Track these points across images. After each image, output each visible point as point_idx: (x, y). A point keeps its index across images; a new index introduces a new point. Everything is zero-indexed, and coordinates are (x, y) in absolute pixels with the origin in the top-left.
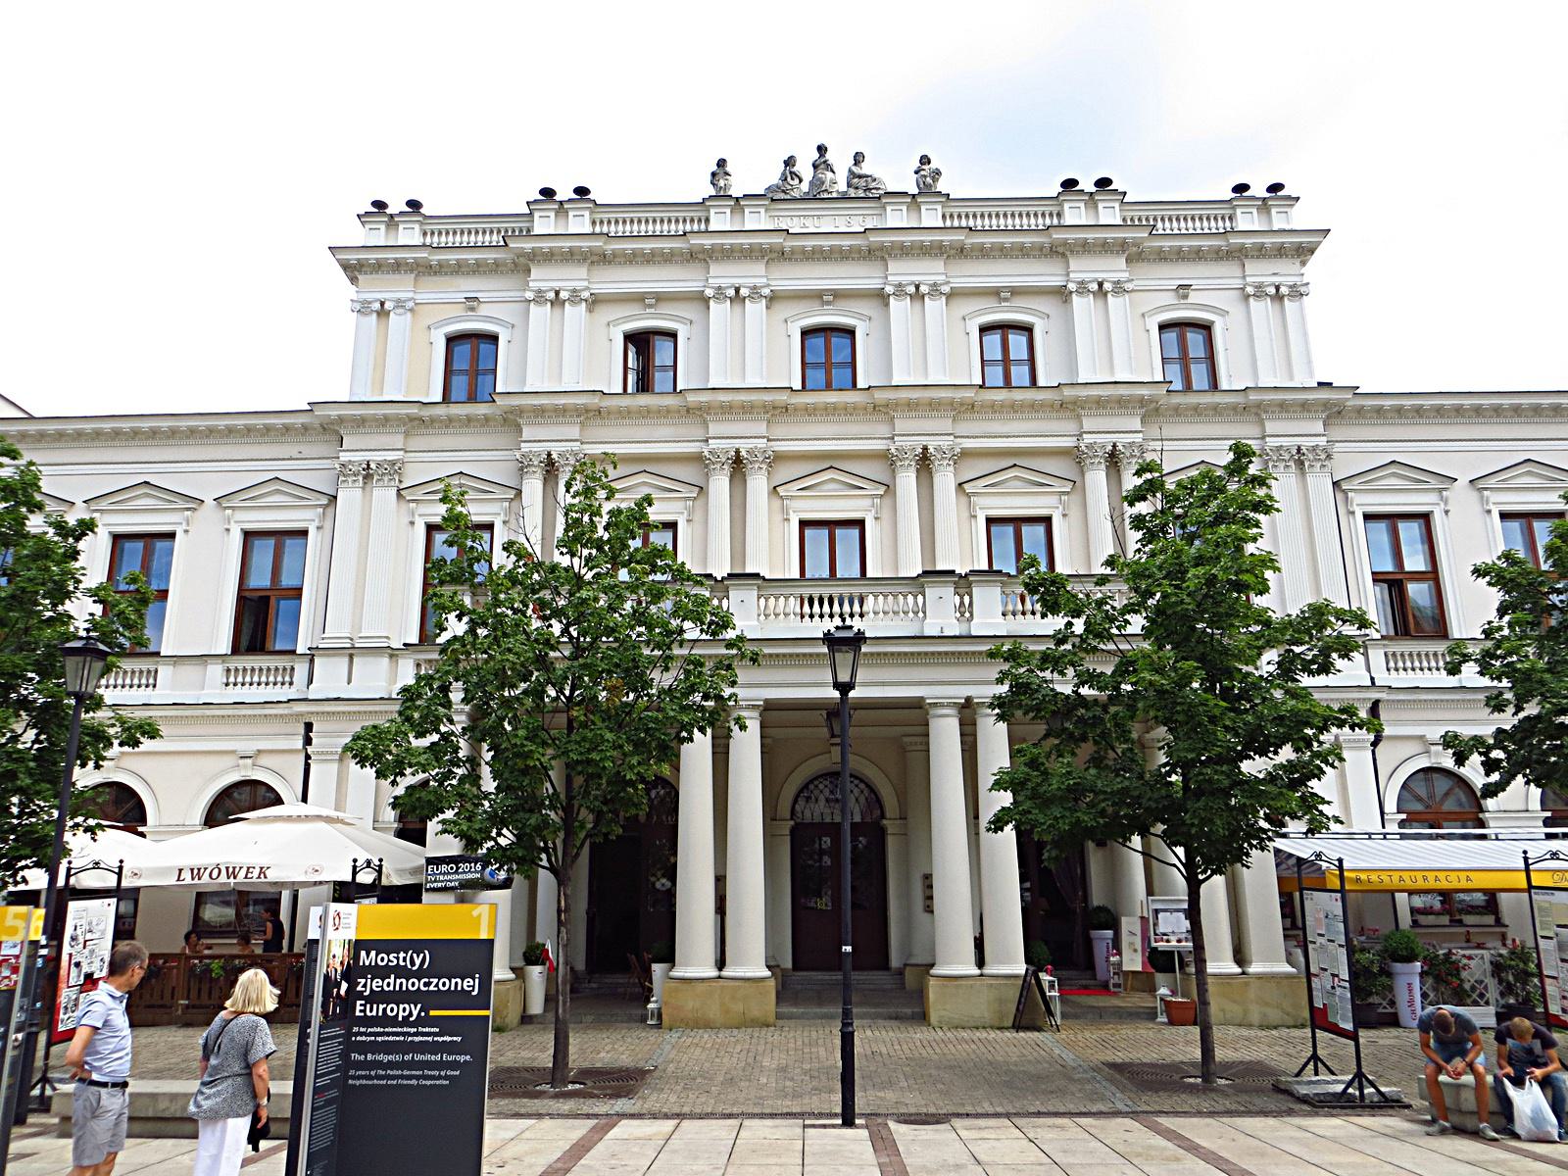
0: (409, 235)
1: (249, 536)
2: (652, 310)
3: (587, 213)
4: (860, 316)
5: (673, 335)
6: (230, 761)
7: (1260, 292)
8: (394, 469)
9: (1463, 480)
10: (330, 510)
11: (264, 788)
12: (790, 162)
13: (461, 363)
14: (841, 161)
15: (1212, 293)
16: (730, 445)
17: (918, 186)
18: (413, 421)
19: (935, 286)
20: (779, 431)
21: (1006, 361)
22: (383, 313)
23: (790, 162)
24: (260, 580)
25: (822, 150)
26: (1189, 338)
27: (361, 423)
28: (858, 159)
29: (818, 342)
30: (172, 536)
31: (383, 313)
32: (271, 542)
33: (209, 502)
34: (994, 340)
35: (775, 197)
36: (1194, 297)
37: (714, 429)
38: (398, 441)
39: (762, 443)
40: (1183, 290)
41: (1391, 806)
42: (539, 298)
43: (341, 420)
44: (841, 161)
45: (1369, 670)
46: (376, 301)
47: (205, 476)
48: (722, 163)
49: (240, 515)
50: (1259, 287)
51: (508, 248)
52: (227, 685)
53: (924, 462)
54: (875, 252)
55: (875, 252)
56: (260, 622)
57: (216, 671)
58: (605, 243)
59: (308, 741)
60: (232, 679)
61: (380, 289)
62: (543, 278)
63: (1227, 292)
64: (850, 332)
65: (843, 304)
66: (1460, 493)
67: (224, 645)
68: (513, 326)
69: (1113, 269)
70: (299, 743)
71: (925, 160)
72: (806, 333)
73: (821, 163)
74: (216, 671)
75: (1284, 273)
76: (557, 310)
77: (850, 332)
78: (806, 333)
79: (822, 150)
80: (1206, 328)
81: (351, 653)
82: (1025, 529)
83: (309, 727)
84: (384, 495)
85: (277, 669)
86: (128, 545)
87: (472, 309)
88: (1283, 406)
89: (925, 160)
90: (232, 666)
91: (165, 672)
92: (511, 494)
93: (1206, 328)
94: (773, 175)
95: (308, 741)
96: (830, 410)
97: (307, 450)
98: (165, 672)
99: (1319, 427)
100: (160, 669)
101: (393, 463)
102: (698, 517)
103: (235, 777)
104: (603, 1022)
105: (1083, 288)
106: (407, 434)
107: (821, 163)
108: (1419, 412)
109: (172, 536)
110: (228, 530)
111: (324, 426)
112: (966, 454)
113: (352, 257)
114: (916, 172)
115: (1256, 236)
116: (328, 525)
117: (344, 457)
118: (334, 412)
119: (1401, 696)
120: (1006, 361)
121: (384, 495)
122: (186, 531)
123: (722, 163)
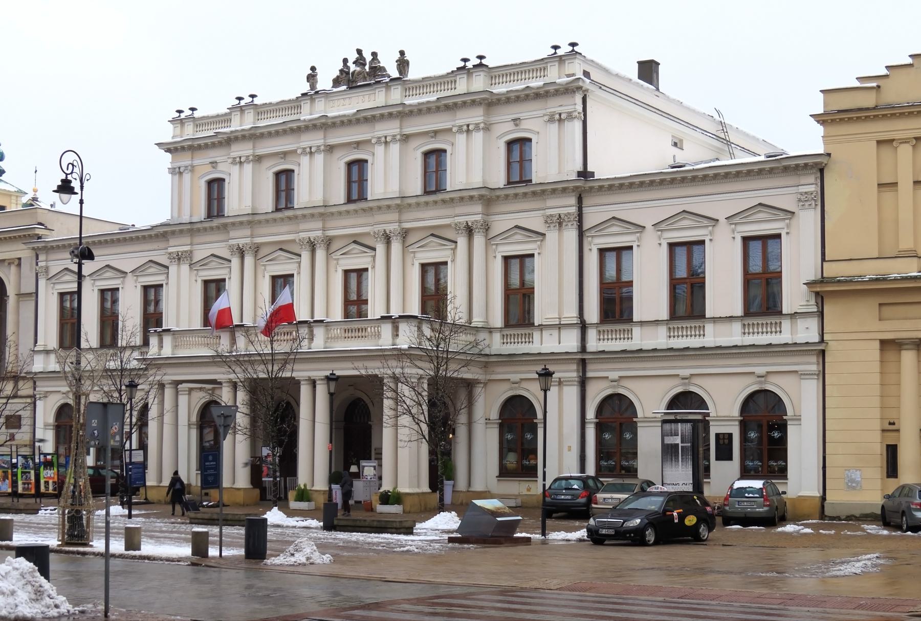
4: (445, 142)
6: (677, 381)
11: (762, 395)
12: (345, 61)
13: (516, 156)
18: (191, 230)
19: (477, 125)
22: (180, 173)
23: (345, 61)
24: (756, 266)
26: (518, 148)
28: (374, 55)
30: (631, 248)
33: (722, 220)
36: (525, 125)
38: (187, 240)
39: (248, 240)
40: (516, 121)
41: (591, 414)
44: (369, 58)
47: (720, 203)
52: (744, 333)
60: (747, 330)
61: (185, 160)
65: (440, 137)
69: (475, 116)
73: (360, 61)
79: (359, 52)
83: (35, 383)
85: (776, 323)
86: (608, 254)
90: (746, 323)
91: (636, 331)
98: (636, 331)
100: (634, 329)
103: (755, 388)
105: (379, 141)
107: (360, 61)
108: (631, 185)
109: (532, 255)
110: (660, 244)
111: (159, 234)
115: (561, 86)
119: (677, 353)
121: (185, 268)
122: (711, 240)
123: (313, 69)
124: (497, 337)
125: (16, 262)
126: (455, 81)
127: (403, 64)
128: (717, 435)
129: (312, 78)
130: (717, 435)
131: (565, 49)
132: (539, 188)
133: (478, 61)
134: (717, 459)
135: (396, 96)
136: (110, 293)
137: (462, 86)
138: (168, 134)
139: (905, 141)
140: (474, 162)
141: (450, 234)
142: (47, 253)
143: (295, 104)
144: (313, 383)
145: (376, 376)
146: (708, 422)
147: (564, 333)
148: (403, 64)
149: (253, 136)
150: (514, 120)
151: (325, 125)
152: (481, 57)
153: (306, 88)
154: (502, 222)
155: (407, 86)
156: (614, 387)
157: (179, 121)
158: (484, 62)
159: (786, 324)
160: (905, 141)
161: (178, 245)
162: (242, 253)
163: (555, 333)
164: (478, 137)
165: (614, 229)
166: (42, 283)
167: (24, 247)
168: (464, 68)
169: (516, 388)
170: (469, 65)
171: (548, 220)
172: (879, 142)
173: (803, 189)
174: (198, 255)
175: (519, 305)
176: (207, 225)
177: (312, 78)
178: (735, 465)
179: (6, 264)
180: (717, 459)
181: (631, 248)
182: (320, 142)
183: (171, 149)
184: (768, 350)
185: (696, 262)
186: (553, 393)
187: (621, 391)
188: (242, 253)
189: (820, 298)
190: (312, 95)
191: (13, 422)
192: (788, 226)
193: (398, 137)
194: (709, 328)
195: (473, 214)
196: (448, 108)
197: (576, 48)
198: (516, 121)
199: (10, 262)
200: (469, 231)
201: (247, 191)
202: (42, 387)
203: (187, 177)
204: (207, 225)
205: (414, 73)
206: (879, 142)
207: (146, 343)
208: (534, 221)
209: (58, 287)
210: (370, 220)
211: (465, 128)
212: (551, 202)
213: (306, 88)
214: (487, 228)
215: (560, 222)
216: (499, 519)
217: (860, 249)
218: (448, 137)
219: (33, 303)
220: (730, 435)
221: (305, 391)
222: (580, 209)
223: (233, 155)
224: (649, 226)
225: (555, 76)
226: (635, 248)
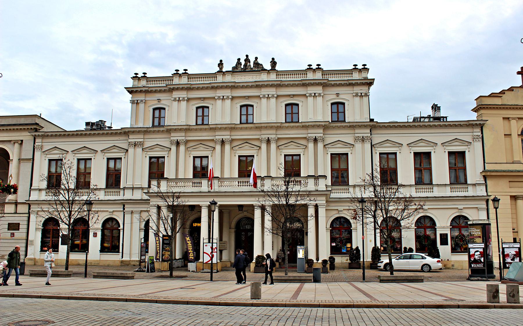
0: (143, 83)
1: (50, 161)
4: (255, 102)
5: (208, 107)
7: (357, 95)
8: (141, 144)
9: (405, 144)
10: (127, 153)
12: (239, 59)
13: (335, 110)
14: (252, 60)
15: (345, 95)
16: (267, 136)
20: (233, 133)
21: (247, 115)
22: (137, 103)
23: (239, 59)
25: (247, 56)
26: (338, 107)
27: (133, 132)
28: (256, 58)
29: (335, 106)
30: (91, 159)
31: (137, 103)
32: (84, 161)
34: (335, 106)
35: (235, 70)
36: (162, 102)
37: (172, 135)
38: (142, 136)
40: (338, 94)
42: (175, 100)
43: (129, 131)
44: (252, 60)
45: (487, 191)
48: (221, 61)
49: (149, 153)
51: (168, 86)
53: (268, 141)
54: (258, 86)
55: (258, 86)
56: (113, 179)
57: (44, 193)
59: (124, 209)
61: (140, 97)
62: (176, 94)
64: (298, 105)
65: (295, 98)
66: (405, 148)
67: (104, 187)
69: (318, 90)
70: (122, 210)
71: (273, 59)
72: (286, 105)
73: (247, 60)
74: (102, 192)
75: (362, 90)
76: (361, 98)
77: (298, 105)
78: (286, 105)
79: (247, 56)
80: (343, 104)
81: (133, 189)
82: (203, 159)
83: (124, 206)
84: (139, 150)
86: (81, 161)
87: (338, 96)
88: (175, 130)
92: (169, 150)
93: (343, 104)
95: (124, 209)
96: (293, 127)
97: (121, 138)
99: (321, 131)
101: (141, 142)
102: (306, 153)
104: (293, 271)
106: (144, 134)
107: (247, 60)
111: (125, 133)
112: (279, 139)
113: (130, 90)
115: (359, 80)
116: (126, 157)
117: (130, 140)
118: (127, 130)
120: (247, 115)
121: (139, 150)
123: (221, 61)
124: (102, 192)
125: (20, 142)
127: (274, 63)
128: (441, 234)
129: (221, 64)
130: (441, 234)
131: (314, 67)
132: (114, 132)
134: (61, 244)
135: (273, 77)
136: (55, 162)
137: (310, 76)
138: (130, 83)
139: (514, 119)
140: (315, 109)
141: (257, 143)
142: (42, 138)
144: (263, 208)
145: (253, 205)
146: (436, 229)
147: (478, 187)
148: (274, 63)
150: (337, 94)
151: (234, 87)
153: (218, 69)
154: (330, 139)
156: (110, 214)
157: (135, 77)
159: (470, 188)
160: (514, 119)
161: (133, 139)
162: (178, 144)
163: (37, 192)
164: (319, 99)
165: (157, 149)
166: (38, 154)
167: (29, 134)
169: (461, 212)
171: (356, 139)
172: (503, 118)
173: (475, 134)
174: (147, 144)
175: (340, 177)
176: (152, 129)
177: (221, 64)
178: (448, 247)
179: (12, 142)
180: (61, 244)
181: (91, 159)
183: (131, 91)
184: (466, 198)
185: (88, 166)
186: (128, 217)
187: (114, 217)
188: (178, 144)
189: (485, 177)
191: (13, 227)
192: (304, 152)
193: (186, 99)
194: (435, 189)
195: (318, 133)
196: (213, 88)
198: (338, 94)
199: (15, 142)
200: (315, 140)
201: (179, 114)
202: (94, 208)
203: (142, 106)
204: (152, 129)
205: (278, 68)
206: (503, 118)
207: (149, 187)
208: (349, 139)
209: (48, 156)
210: (213, 134)
212: (357, 131)
214: (323, 140)
215: (363, 140)
216: (242, 273)
217: (498, 159)
219: (31, 164)
220: (447, 234)
221: (258, 213)
222: (482, 133)
223: (174, 96)
224: (99, 151)
225: (356, 76)
226: (93, 159)
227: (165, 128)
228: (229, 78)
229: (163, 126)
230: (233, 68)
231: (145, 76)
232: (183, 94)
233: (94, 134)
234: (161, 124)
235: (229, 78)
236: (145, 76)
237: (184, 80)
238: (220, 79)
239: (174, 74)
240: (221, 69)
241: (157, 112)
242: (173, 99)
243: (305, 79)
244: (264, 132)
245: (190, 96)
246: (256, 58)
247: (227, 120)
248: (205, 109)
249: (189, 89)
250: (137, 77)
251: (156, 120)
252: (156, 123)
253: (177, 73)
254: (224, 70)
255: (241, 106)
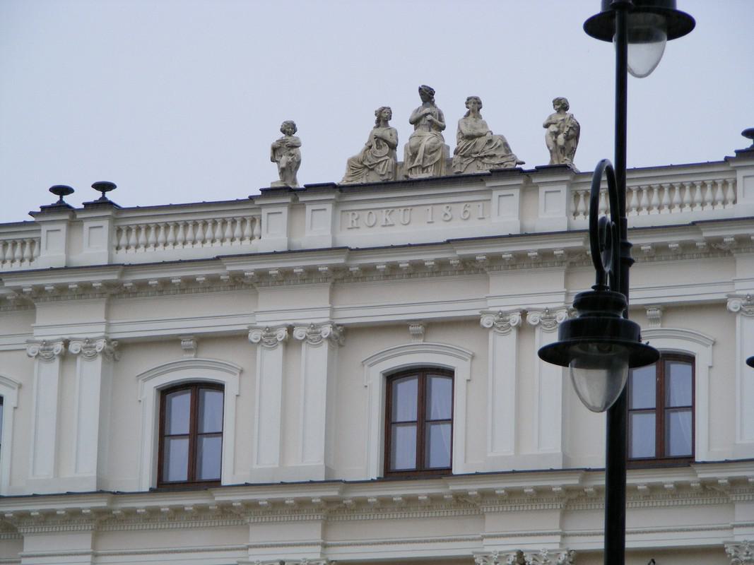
2: (420, 341)
3: (105, 223)
12: (383, 117)
17: (442, 136)
23: (383, 117)
25: (427, 95)
28: (474, 105)
42: (45, 352)
44: (452, 111)
46: (516, 311)
48: (289, 129)
50: (503, 316)
58: (348, 259)
62: (53, 324)
63: (12, 354)
65: (438, 338)
68: (20, 386)
73: (428, 119)
79: (427, 95)
89: (562, 106)
94: (356, 140)
107: (428, 119)
114: (547, 126)
123: (289, 129)
126: (735, 184)
129: (286, 149)
131: (82, 195)
133: (96, 195)
143: (242, 211)
149: (118, 287)
151: (345, 270)
152: (104, 187)
155: (123, 223)
158: (110, 195)
168: (61, 207)
170: (72, 200)
177: (286, 149)
182: (97, 331)
190: (287, 192)
197: (110, 195)
210: (470, 527)
211: (282, 333)
213: (271, 177)
218: (463, 341)
223: (40, 334)
227: (220, 497)
228: (318, 228)
229: (446, 472)
230: (357, 165)
231: (104, 204)
232: (85, 323)
233: (410, 501)
234: (436, 462)
235: (318, 228)
236: (104, 204)
237: (94, 246)
238: (274, 231)
239: (46, 210)
240: (289, 170)
241: (181, 403)
242: (34, 349)
243: (26, 266)
244: (495, 523)
245: (125, 330)
246: (474, 105)
247: (81, 473)
248: (437, 383)
249: (118, 287)
250: (68, 208)
251: (406, 439)
252: (178, 471)
253: (61, 207)
254: (303, 178)
255: (392, 378)
